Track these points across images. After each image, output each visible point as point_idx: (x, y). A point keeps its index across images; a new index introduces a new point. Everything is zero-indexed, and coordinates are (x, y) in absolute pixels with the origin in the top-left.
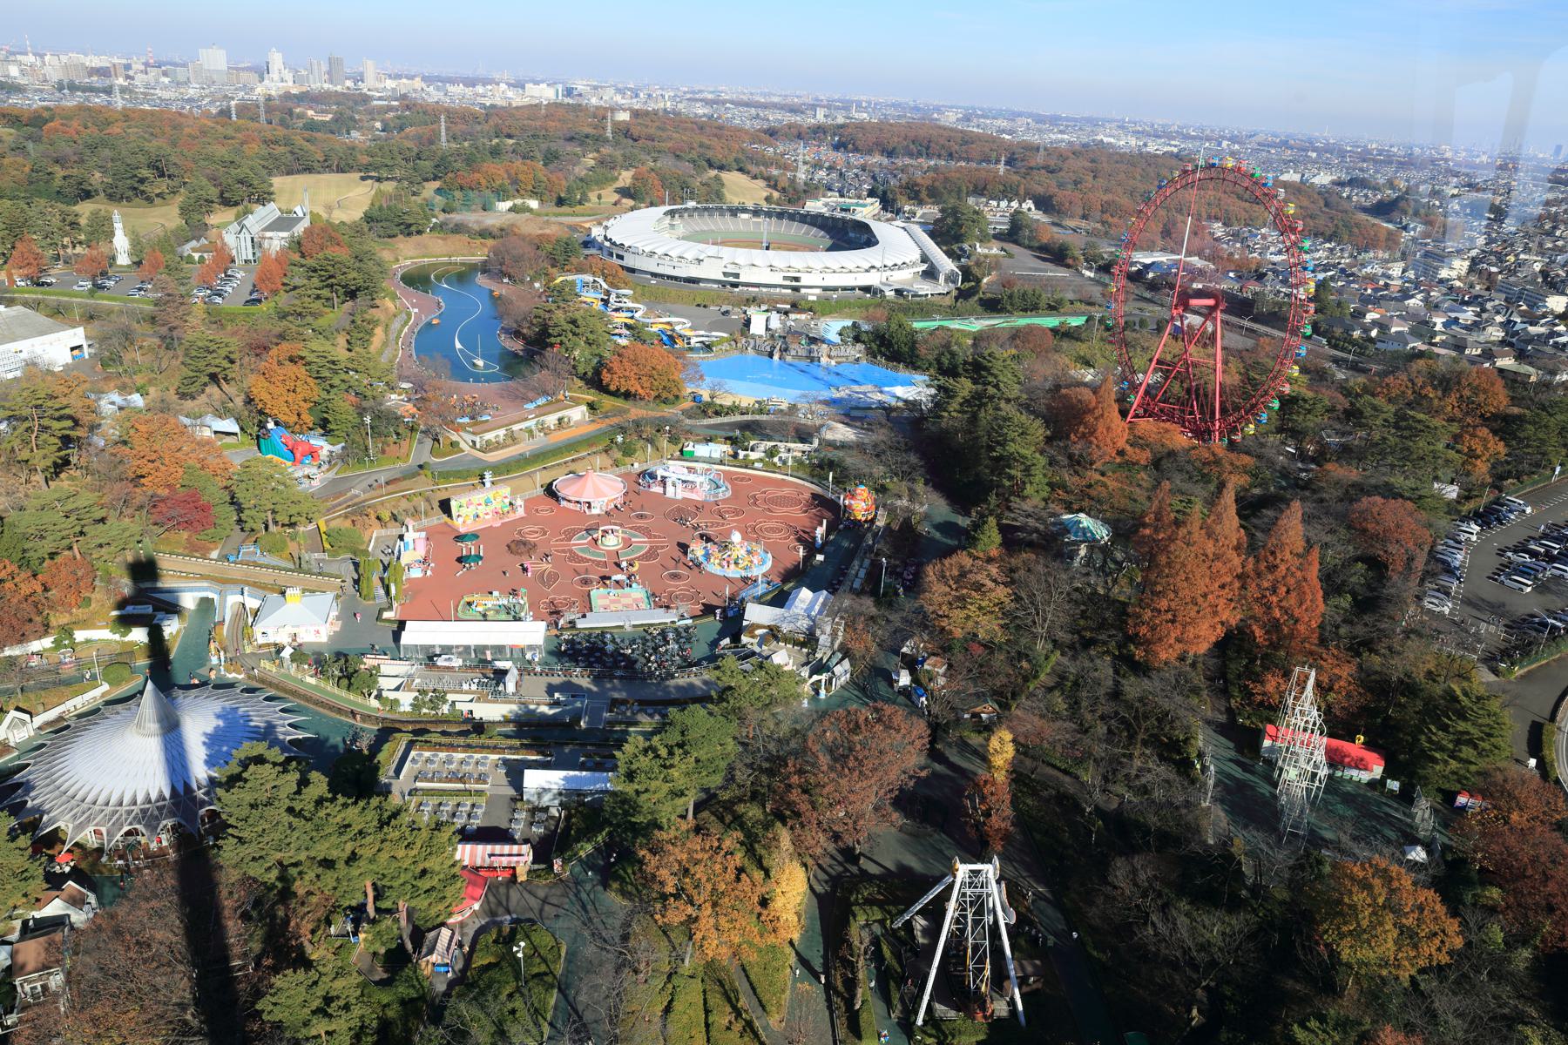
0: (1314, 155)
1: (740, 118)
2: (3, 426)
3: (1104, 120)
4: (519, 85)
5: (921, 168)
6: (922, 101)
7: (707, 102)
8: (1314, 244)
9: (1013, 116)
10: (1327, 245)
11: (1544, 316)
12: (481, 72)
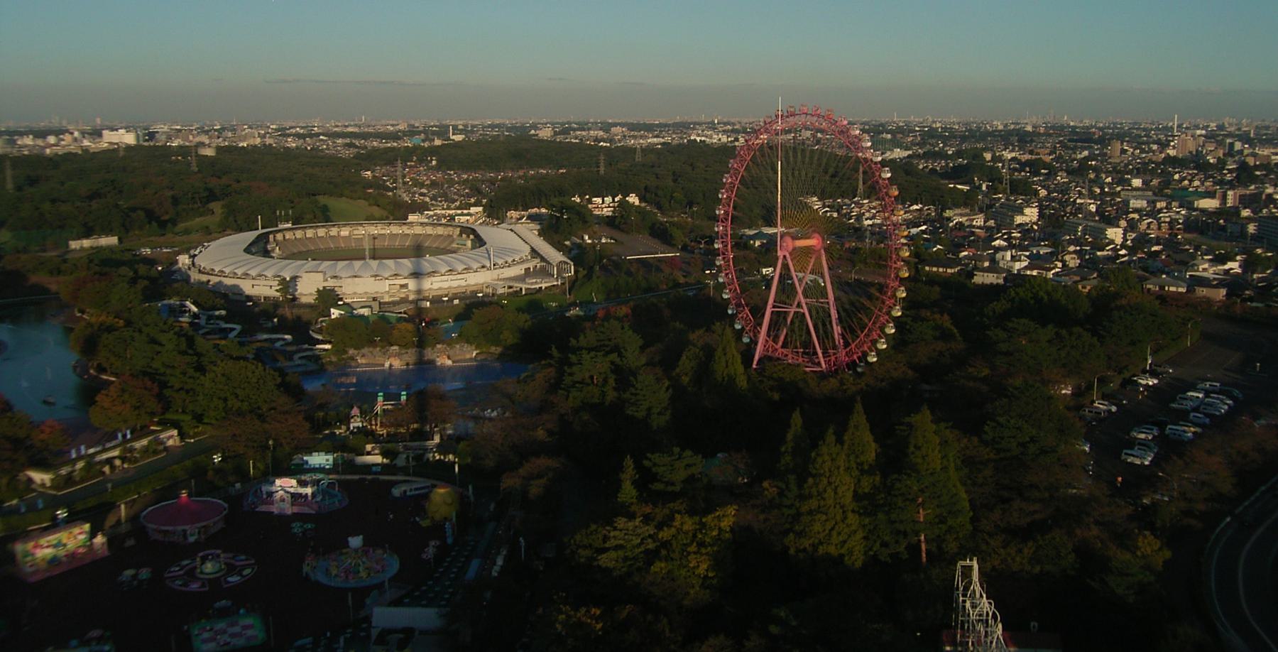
0: (889, 136)
1: (339, 148)
2: (2, 237)
3: (695, 124)
4: (96, 134)
5: (518, 175)
6: (518, 120)
7: (298, 136)
8: (373, 449)
9: (606, 127)
10: (915, 207)
11: (1108, 244)
12: (55, 122)
